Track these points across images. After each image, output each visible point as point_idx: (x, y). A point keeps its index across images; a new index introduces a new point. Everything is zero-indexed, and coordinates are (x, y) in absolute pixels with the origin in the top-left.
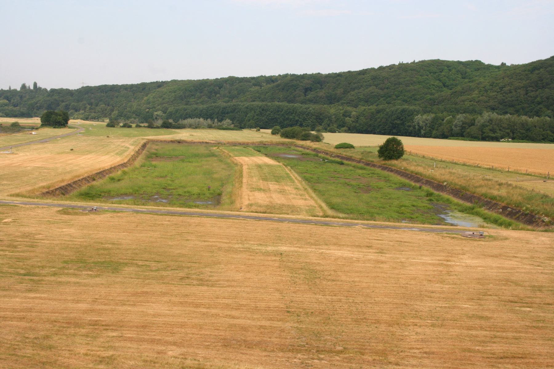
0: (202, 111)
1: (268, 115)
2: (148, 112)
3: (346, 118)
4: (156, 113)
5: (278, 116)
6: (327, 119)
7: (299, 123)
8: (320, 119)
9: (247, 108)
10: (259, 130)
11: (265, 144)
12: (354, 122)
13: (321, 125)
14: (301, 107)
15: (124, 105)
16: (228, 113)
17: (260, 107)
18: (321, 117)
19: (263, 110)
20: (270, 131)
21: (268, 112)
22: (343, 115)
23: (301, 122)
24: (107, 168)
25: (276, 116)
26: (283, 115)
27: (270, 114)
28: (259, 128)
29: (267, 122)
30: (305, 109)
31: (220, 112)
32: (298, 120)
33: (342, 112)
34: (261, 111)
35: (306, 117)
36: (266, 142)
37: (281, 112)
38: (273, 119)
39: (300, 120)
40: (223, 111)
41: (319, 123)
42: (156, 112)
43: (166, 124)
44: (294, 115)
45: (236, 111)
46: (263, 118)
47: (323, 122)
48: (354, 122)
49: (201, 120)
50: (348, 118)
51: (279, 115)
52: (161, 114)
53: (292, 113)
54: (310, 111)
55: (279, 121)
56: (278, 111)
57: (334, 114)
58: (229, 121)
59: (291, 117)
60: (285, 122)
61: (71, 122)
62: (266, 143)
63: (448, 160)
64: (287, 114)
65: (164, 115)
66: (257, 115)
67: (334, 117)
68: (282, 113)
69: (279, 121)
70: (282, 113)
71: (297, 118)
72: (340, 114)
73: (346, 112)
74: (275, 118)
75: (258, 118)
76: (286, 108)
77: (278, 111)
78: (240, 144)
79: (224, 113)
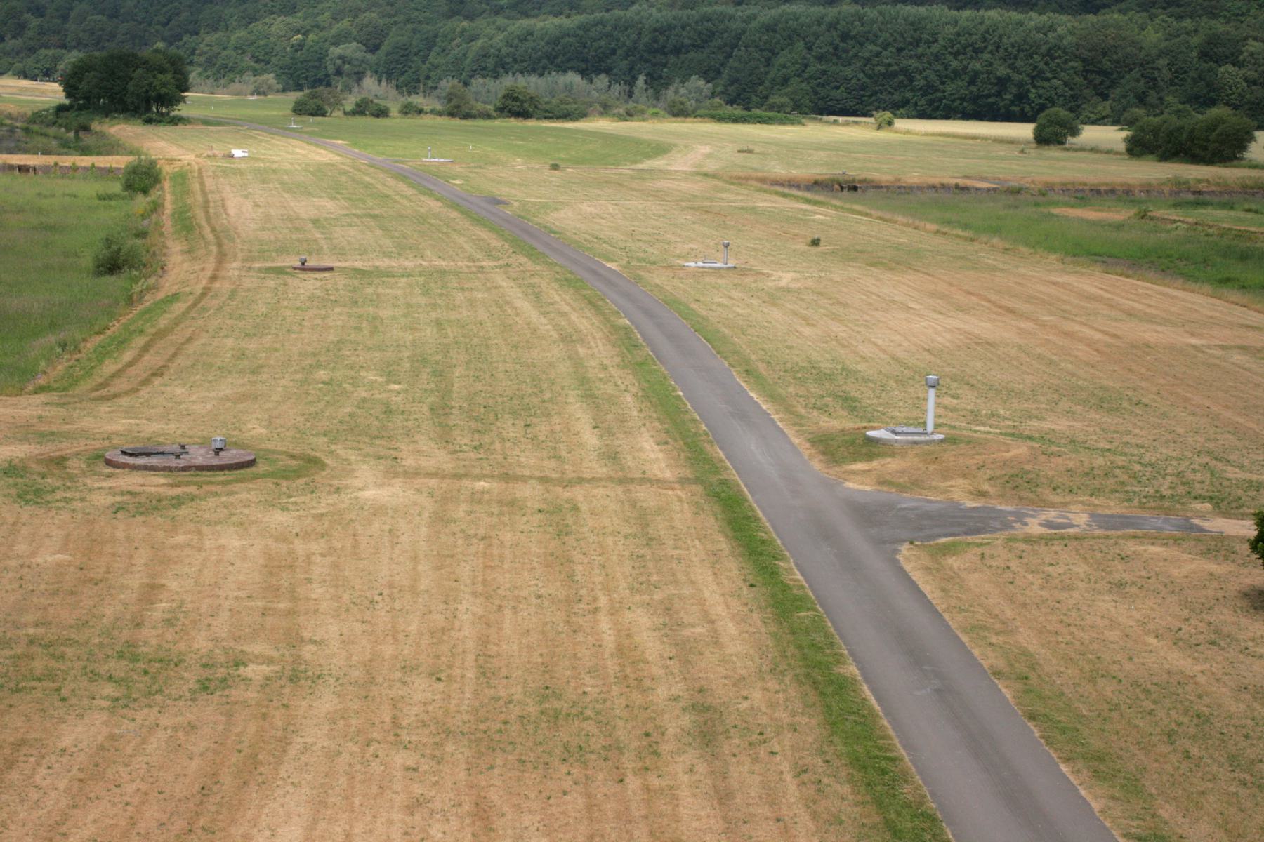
0: (556, 41)
1: (868, 60)
2: (301, 46)
3: (1222, 69)
4: (336, 51)
5: (914, 63)
6: (1136, 73)
7: (1014, 90)
8: (1101, 72)
9: (770, 28)
10: (890, 123)
11: (1200, 193)
12: (1254, 83)
13: (1105, 97)
14: (1020, 24)
15: (185, 15)
16: (677, 51)
17: (832, 26)
18: (1106, 64)
19: (845, 37)
20: (1025, 131)
21: (871, 47)
22: (1204, 55)
23: (1020, 85)
24: (1207, 288)
25: (904, 63)
26: (937, 57)
27: (878, 54)
28: (888, 115)
29: (863, 87)
30: (1038, 30)
31: (641, 47)
32: (1008, 79)
33: (1195, 41)
34: (837, 41)
35: (1041, 65)
36: (1199, 181)
37: (929, 43)
38: (894, 75)
39: (1016, 77)
40: (655, 41)
41: (1095, 88)
42: (336, 44)
43: (516, 99)
44: (986, 56)
45: (717, 42)
46: (848, 72)
47: (1113, 85)
48: (1254, 83)
49: (573, 78)
50: (1230, 68)
51: (919, 57)
52: (359, 55)
53: (977, 51)
54: (1061, 38)
55: (920, 82)
56: (916, 43)
57: (1162, 53)
58: (701, 83)
59: (976, 65)
60: (950, 88)
61: (195, 101)
62: (1201, 187)
63: (913, 177)
64: (956, 55)
65: (369, 56)
66: (820, 58)
67: (1162, 62)
68: (935, 48)
69: (920, 82)
70: (935, 48)
71: (1002, 71)
72: (1190, 49)
73: (1213, 41)
74: (904, 71)
75: (824, 72)
76: (949, 30)
77: (916, 43)
78: (1099, 192)
79: (662, 51)
